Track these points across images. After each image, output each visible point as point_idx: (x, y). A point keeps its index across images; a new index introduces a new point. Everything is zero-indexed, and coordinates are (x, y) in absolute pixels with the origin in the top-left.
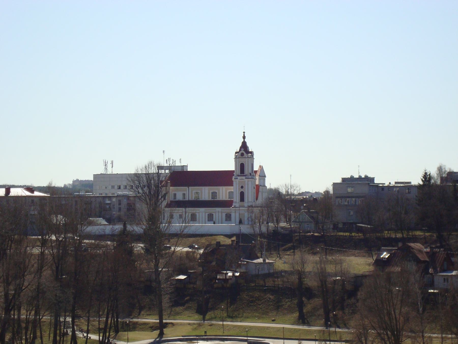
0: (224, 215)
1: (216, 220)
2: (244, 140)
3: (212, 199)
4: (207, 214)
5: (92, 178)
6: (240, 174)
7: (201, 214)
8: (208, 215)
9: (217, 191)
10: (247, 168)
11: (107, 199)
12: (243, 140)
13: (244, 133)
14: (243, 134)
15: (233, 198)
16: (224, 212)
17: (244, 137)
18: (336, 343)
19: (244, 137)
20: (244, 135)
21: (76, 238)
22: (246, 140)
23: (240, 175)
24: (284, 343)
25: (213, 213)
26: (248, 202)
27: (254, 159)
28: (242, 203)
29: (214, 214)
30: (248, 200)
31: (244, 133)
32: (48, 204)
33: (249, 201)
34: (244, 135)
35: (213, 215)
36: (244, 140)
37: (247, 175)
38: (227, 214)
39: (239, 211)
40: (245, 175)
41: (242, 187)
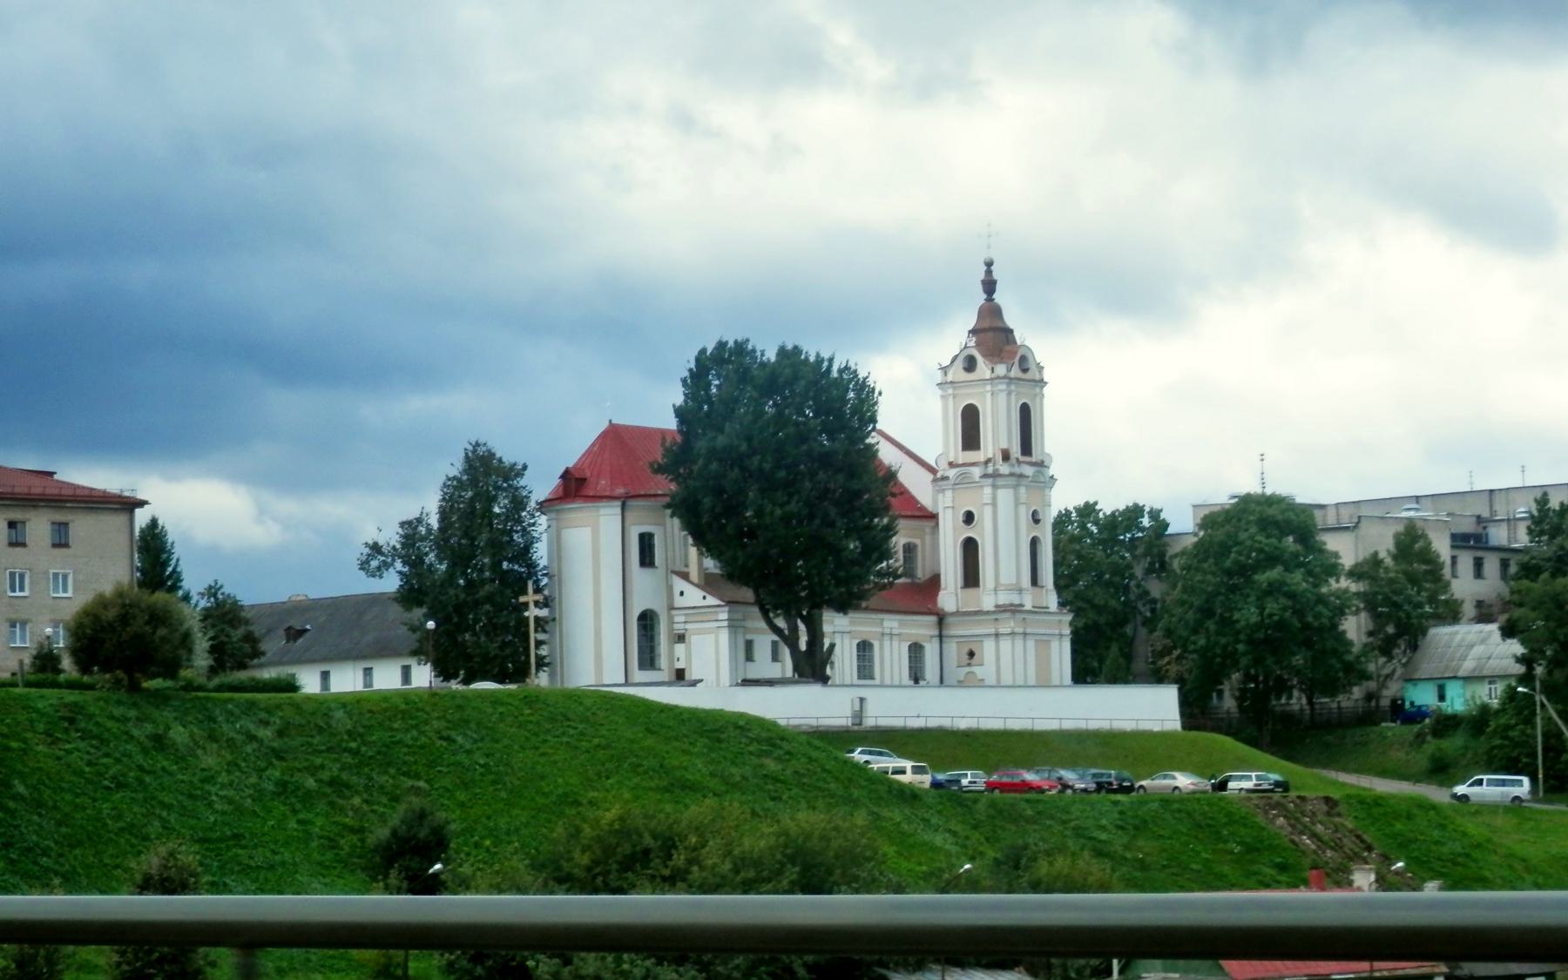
3: (365, 686)
5: (417, 644)
10: (1023, 721)
13: (989, 264)
17: (989, 286)
18: (1384, 967)
19: (989, 286)
20: (989, 272)
22: (996, 275)
25: (873, 641)
26: (995, 590)
27: (1046, 383)
28: (971, 591)
29: (876, 644)
30: (665, 529)
31: (989, 264)
32: (78, 800)
33: (999, 491)
34: (989, 272)
41: (969, 518)
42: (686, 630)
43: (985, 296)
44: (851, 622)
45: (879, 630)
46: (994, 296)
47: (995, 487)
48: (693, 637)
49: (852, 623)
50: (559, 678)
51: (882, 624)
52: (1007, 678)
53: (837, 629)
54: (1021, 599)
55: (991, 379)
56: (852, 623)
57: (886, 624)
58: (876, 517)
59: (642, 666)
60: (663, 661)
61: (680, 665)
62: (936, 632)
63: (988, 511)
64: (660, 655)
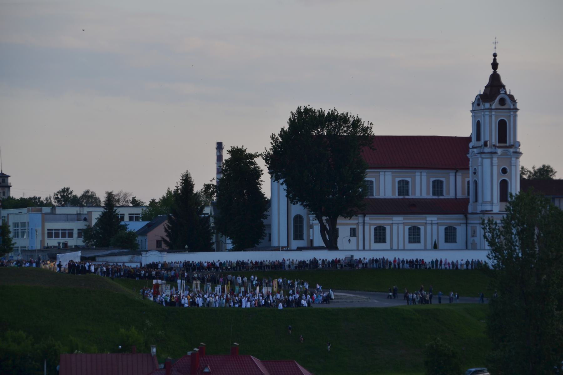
0: (442, 229)
1: (438, 241)
2: (495, 72)
4: (407, 228)
6: (499, 143)
7: (395, 227)
8: (410, 229)
9: (409, 179)
11: (409, 294)
12: (491, 71)
13: (495, 55)
14: (493, 57)
15: (135, 220)
16: (442, 224)
17: (495, 65)
19: (495, 65)
20: (495, 60)
21: (245, 191)
22: (498, 61)
23: (497, 145)
24: (1, 163)
29: (422, 228)
31: (495, 55)
34: (495, 60)
35: (419, 229)
36: (495, 72)
37: (513, 145)
38: (411, 227)
39: (427, 221)
40: (508, 145)
41: (504, 171)
42: (312, 223)
43: (493, 71)
44: (404, 218)
45: (425, 221)
46: (497, 71)
47: (482, 158)
48: (315, 226)
49: (404, 219)
50: (117, 251)
51: (426, 219)
52: (401, 247)
53: (394, 222)
54: (492, 208)
55: (484, 109)
56: (404, 219)
57: (428, 219)
58: (224, 179)
59: (296, 238)
60: (305, 236)
61: (311, 238)
62: (465, 222)
63: (480, 167)
64: (304, 234)
